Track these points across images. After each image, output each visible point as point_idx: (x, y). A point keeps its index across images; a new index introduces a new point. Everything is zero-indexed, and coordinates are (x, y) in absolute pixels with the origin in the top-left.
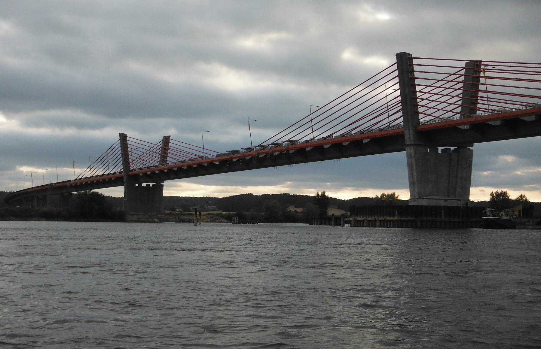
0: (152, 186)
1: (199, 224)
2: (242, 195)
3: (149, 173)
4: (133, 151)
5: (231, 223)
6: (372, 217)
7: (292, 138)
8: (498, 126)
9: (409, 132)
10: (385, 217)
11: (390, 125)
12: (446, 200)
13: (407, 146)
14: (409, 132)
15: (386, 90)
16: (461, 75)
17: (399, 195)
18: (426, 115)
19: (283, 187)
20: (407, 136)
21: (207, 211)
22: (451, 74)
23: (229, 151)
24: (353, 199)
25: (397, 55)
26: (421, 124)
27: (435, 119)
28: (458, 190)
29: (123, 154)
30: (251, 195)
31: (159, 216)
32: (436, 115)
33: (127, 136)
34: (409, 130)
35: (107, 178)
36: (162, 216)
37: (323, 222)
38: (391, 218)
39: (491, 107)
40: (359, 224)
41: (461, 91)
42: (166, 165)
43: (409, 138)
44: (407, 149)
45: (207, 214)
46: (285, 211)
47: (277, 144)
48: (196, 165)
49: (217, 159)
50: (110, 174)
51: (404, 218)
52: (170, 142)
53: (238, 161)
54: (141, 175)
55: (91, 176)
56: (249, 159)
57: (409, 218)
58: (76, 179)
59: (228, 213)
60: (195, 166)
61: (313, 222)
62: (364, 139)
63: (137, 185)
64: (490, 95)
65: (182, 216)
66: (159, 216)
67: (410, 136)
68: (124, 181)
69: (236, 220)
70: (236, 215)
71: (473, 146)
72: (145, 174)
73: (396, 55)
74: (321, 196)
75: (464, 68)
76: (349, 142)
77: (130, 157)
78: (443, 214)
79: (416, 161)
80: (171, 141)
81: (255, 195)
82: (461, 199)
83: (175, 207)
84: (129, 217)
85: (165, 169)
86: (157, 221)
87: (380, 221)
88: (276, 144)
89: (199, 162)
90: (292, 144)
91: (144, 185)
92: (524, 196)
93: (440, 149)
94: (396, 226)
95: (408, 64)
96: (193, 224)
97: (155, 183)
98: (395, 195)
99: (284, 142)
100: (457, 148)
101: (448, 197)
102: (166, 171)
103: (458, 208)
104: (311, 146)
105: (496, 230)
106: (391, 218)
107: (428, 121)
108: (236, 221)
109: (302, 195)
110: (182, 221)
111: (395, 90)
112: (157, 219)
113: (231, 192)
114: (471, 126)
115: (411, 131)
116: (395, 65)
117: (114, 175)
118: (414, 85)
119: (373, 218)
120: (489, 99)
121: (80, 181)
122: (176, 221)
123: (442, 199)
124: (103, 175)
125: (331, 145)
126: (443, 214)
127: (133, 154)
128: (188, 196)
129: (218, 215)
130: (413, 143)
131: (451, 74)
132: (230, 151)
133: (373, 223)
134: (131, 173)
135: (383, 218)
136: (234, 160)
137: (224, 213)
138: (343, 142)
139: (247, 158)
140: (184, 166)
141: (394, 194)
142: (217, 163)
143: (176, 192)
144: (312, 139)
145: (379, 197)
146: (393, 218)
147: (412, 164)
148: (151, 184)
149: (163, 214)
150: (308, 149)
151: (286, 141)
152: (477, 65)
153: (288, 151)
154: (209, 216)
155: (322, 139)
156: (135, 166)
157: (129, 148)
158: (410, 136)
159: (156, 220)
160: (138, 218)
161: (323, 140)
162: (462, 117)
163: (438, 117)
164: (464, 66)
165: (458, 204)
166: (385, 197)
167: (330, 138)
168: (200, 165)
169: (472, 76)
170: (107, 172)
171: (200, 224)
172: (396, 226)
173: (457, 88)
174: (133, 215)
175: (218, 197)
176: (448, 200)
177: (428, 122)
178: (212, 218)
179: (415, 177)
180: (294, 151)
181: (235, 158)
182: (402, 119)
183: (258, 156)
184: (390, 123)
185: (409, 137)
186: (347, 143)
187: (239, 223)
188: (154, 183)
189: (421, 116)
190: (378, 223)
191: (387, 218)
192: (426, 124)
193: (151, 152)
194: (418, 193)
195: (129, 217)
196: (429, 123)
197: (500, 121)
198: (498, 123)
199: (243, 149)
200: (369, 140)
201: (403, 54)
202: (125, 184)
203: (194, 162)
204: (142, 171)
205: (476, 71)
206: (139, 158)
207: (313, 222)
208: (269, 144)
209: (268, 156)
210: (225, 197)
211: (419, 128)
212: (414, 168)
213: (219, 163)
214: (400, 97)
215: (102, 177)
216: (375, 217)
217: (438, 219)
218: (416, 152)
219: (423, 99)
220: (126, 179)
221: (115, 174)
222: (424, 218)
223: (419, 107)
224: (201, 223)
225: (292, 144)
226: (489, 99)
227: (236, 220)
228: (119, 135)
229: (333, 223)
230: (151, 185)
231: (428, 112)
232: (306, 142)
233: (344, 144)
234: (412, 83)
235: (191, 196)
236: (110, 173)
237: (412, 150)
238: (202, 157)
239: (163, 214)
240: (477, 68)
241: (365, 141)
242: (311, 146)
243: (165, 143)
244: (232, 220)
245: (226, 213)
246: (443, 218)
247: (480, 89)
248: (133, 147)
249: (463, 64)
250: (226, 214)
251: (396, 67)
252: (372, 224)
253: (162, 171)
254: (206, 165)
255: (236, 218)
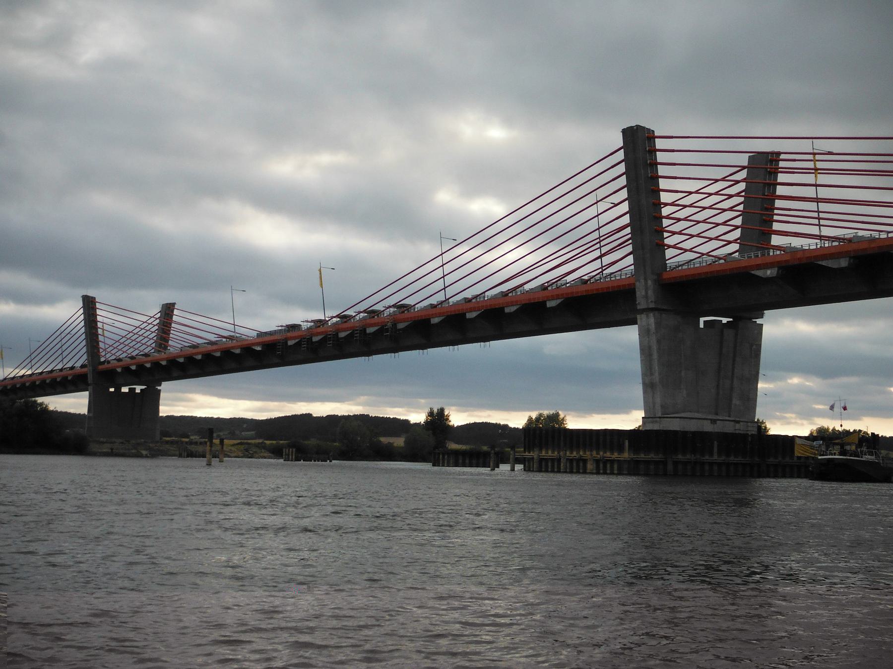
0: (139, 391)
1: (220, 462)
2: (295, 415)
3: (133, 368)
4: (106, 327)
5: (283, 460)
6: (572, 453)
7: (402, 300)
8: (841, 270)
9: (646, 283)
10: (601, 453)
11: (604, 272)
12: (714, 421)
13: (642, 311)
14: (646, 283)
15: (596, 203)
16: (737, 227)
17: (565, 416)
18: (683, 251)
19: (358, 404)
20: (640, 293)
21: (239, 439)
22: (690, 193)
23: (282, 326)
24: (467, 424)
25: (624, 132)
26: (668, 270)
27: (700, 260)
28: (736, 401)
29: (88, 333)
30: (309, 415)
31: (151, 445)
32: (704, 249)
33: (97, 300)
34: (646, 280)
35: (59, 376)
36: (156, 446)
37: (461, 461)
38: (615, 455)
39: (826, 232)
40: (556, 466)
41: (742, 199)
42: (165, 353)
43: (646, 297)
44: (641, 319)
45: (238, 444)
46: (375, 440)
47: (374, 312)
48: (220, 352)
49: (260, 340)
50: (65, 368)
51: (642, 456)
52: (174, 313)
53: (298, 344)
54: (119, 370)
55: (31, 373)
56: (319, 340)
57: (652, 456)
58: (5, 379)
59: (274, 442)
60: (218, 354)
61: (441, 460)
62: (549, 300)
63: (112, 390)
64: (823, 207)
65: (193, 446)
66: (151, 445)
67: (647, 293)
68: (89, 382)
69: (292, 455)
70: (290, 446)
71: (762, 318)
72: (127, 369)
73: (621, 132)
74: (436, 416)
75: (743, 168)
76: (518, 307)
77: (101, 338)
78: (715, 450)
79: (659, 342)
80: (176, 312)
81: (315, 416)
82: (741, 420)
83: (190, 434)
84: (94, 447)
85: (162, 359)
86: (146, 455)
87: (597, 462)
88: (372, 313)
89: (224, 346)
90: (403, 312)
91: (125, 390)
92: (763, 421)
93: (702, 320)
94: (625, 472)
95: (646, 149)
96: (203, 461)
97: (146, 387)
98: (559, 415)
99: (388, 308)
100: (731, 320)
101: (717, 415)
102: (164, 363)
103: (744, 437)
104: (439, 315)
105: (853, 484)
106: (615, 455)
107: (685, 262)
108: (290, 457)
109: (388, 417)
110: (191, 455)
111: (613, 205)
112: (147, 450)
113: (272, 411)
114: (780, 271)
115: (650, 282)
116: (620, 151)
117: (71, 372)
118: (657, 191)
119: (575, 454)
120: (822, 215)
121: (11, 382)
122: (180, 456)
123: (707, 419)
124: (52, 371)
125: (481, 311)
126: (715, 450)
127: (106, 334)
128: (210, 416)
129: (257, 446)
130: (652, 306)
131: (716, 181)
132: (284, 326)
133: (575, 464)
134: (101, 367)
135: (597, 454)
136: (290, 343)
137: (268, 442)
138: (506, 307)
139: (315, 339)
140: (197, 355)
141: (557, 415)
142: (259, 348)
143: (186, 409)
144: (442, 302)
145: (455, 426)
146: (619, 455)
147: (650, 348)
148: (138, 389)
149: (157, 442)
150: (435, 320)
151: (393, 306)
152: (771, 161)
153: (395, 325)
154: (242, 447)
155: (464, 302)
156: (109, 353)
157: (98, 323)
158: (647, 293)
159: (144, 452)
160: (112, 449)
161: (466, 302)
162: (752, 255)
163: (707, 254)
164: (746, 164)
165: (736, 430)
166: (542, 418)
167: (478, 300)
168: (227, 353)
169: (763, 183)
170: (59, 367)
171: (221, 461)
172: (625, 472)
173: (726, 207)
174: (103, 443)
175: (258, 419)
176: (718, 422)
177: (683, 264)
178: (247, 450)
179: (657, 374)
180: (406, 324)
181: (293, 340)
182: (630, 260)
183: (337, 334)
184: (604, 268)
185: (645, 295)
186: (513, 309)
187: (297, 459)
188: (143, 387)
189: (669, 253)
190: (590, 466)
191: (605, 455)
192: (680, 268)
193: (138, 329)
194: (662, 406)
195: (94, 447)
196: (684, 267)
197: (848, 259)
198: (844, 263)
199: (307, 321)
200: (559, 301)
201: (637, 128)
202: (90, 388)
203: (214, 347)
204: (121, 363)
205: (769, 172)
206: (121, 341)
207: (441, 460)
208: (360, 312)
209: (357, 334)
210: (269, 418)
211: (665, 276)
212: (655, 356)
213: (262, 348)
214: (628, 215)
215: (50, 375)
216: (578, 453)
217: (707, 457)
218: (658, 325)
219: (674, 233)
220: (91, 378)
221: (73, 369)
222: (680, 457)
223: (666, 235)
224: (225, 459)
225: (403, 312)
226: (822, 215)
227: (292, 455)
228: (81, 298)
229: (491, 464)
230: (138, 391)
231: (687, 245)
232: (432, 308)
233: (507, 310)
234: (654, 187)
235: (215, 417)
236: (65, 367)
237: (652, 320)
238: (230, 338)
239: (157, 442)
240: (771, 167)
241: (551, 304)
242: (439, 315)
243: (165, 315)
244: (284, 454)
245: (271, 442)
246: (715, 457)
247: (775, 206)
248: (106, 320)
249: (744, 160)
250: (272, 444)
251: (621, 155)
252: (553, 467)
253: (156, 364)
254: (238, 351)
255: (287, 450)
